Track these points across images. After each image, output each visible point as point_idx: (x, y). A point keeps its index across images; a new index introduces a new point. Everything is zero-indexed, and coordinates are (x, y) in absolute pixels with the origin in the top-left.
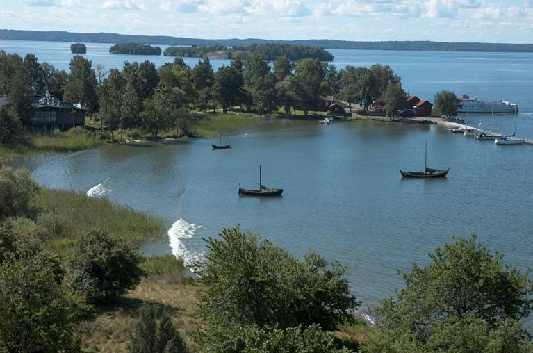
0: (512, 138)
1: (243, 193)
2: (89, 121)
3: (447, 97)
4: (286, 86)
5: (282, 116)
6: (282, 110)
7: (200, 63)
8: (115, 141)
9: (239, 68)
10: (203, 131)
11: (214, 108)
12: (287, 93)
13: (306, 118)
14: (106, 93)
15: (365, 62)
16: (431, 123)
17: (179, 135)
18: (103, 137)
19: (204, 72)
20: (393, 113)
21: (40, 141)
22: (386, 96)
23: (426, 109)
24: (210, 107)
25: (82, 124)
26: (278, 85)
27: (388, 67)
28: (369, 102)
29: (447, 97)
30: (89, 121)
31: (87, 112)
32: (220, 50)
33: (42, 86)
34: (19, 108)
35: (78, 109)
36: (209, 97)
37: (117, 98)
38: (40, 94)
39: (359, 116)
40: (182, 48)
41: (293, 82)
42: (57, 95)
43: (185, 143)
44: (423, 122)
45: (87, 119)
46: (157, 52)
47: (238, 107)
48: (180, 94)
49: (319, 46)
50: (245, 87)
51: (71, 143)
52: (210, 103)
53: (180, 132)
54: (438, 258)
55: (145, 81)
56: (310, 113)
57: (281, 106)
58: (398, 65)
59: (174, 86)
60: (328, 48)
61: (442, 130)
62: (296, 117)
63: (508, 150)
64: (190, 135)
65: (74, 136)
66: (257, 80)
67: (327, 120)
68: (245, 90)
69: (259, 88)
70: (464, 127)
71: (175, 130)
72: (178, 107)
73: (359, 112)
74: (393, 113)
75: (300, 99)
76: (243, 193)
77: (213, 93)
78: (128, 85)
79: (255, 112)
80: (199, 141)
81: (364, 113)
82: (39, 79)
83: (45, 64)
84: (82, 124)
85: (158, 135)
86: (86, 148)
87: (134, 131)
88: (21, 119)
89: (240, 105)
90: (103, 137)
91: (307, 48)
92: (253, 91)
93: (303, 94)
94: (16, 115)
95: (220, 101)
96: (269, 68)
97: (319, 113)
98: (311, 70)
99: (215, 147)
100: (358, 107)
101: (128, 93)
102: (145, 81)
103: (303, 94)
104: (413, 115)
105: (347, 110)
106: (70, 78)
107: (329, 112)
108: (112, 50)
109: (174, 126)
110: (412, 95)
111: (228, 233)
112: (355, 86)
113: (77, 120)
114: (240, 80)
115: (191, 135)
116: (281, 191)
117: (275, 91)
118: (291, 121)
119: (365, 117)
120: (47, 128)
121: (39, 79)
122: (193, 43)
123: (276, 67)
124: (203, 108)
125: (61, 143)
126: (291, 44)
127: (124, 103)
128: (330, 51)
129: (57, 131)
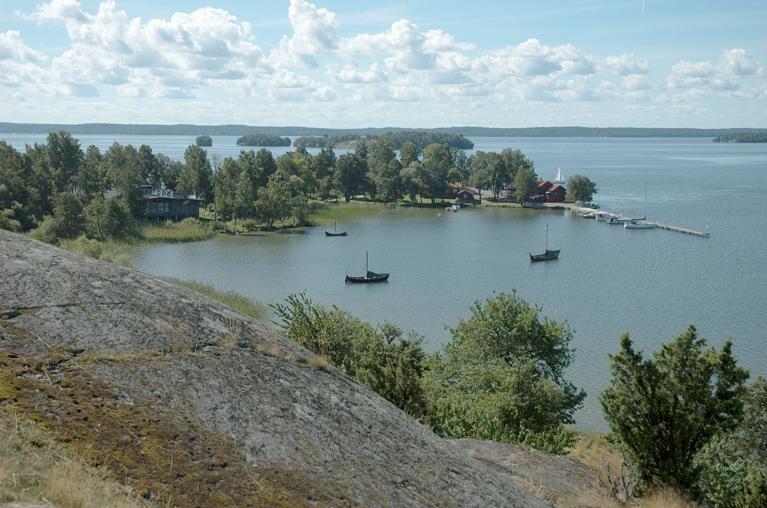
0: (643, 222)
1: (351, 280)
2: (203, 213)
3: (580, 182)
4: (411, 173)
5: (408, 205)
6: (407, 198)
7: (323, 152)
8: (228, 232)
9: (364, 156)
10: (322, 220)
11: (336, 198)
12: (413, 180)
13: (433, 206)
14: (220, 182)
15: (497, 147)
16: (563, 208)
17: (295, 225)
18: (217, 228)
19: (327, 161)
20: (526, 199)
21: (150, 232)
22: (518, 181)
23: (559, 195)
24: (333, 197)
25: (196, 216)
26: (402, 172)
27: (519, 151)
28: (499, 187)
29: (580, 182)
30: (203, 213)
31: (201, 204)
32: (352, 139)
33: (157, 177)
34: (130, 199)
35: (193, 200)
36: (330, 186)
37: (232, 187)
38: (156, 186)
39: (489, 203)
40: (309, 138)
41: (418, 168)
42: (171, 186)
43: (302, 232)
44: (556, 208)
45: (201, 210)
46: (287, 143)
47: (362, 196)
48: (298, 182)
49: (458, 134)
50: (370, 174)
51: (181, 234)
52: (332, 192)
53: (297, 221)
54: (477, 310)
55: (261, 169)
56: (438, 200)
57: (406, 194)
58: (528, 149)
59: (291, 174)
60: (470, 136)
61: (575, 215)
62: (422, 205)
63: (639, 233)
64: (305, 224)
65: (187, 227)
66: (381, 167)
67: (454, 207)
68: (368, 178)
69: (383, 175)
70: (596, 212)
71: (291, 219)
72: (294, 196)
73: (489, 199)
74: (526, 199)
75: (427, 186)
76: (351, 280)
77: (334, 182)
78: (243, 174)
79: (379, 201)
80: (315, 230)
81: (494, 200)
82: (153, 171)
83: (160, 155)
84: (196, 216)
85: (274, 225)
86: (199, 239)
87: (249, 221)
88: (132, 211)
89: (364, 194)
90: (217, 228)
91: (446, 135)
92: (378, 180)
93: (429, 181)
94: (126, 207)
95: (342, 191)
96: (395, 155)
97: (446, 200)
98: (439, 156)
99: (328, 234)
100: (489, 193)
101: (242, 182)
102: (261, 169)
103: (429, 181)
104: (545, 201)
105: (476, 197)
106: (186, 169)
107: (457, 199)
108: (240, 142)
109: (290, 215)
110: (545, 180)
111: (295, 299)
112: (485, 172)
113: (192, 210)
114: (363, 167)
115: (308, 225)
116: (387, 276)
117: (400, 179)
118: (418, 209)
119: (495, 204)
120: (158, 219)
121: (153, 171)
122: (325, 133)
123: (402, 154)
124: (324, 197)
125: (171, 234)
126: (450, 133)
127: (238, 192)
128: (470, 139)
129: (169, 222)
